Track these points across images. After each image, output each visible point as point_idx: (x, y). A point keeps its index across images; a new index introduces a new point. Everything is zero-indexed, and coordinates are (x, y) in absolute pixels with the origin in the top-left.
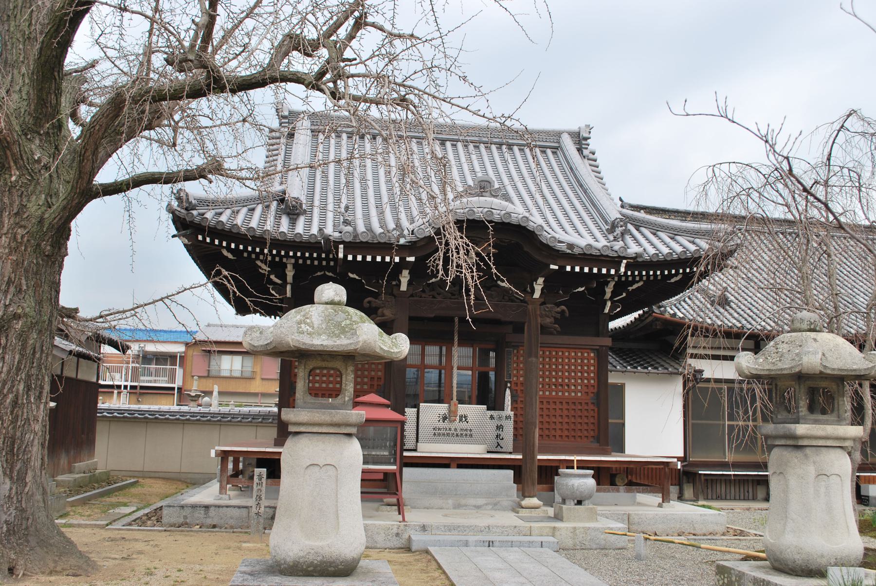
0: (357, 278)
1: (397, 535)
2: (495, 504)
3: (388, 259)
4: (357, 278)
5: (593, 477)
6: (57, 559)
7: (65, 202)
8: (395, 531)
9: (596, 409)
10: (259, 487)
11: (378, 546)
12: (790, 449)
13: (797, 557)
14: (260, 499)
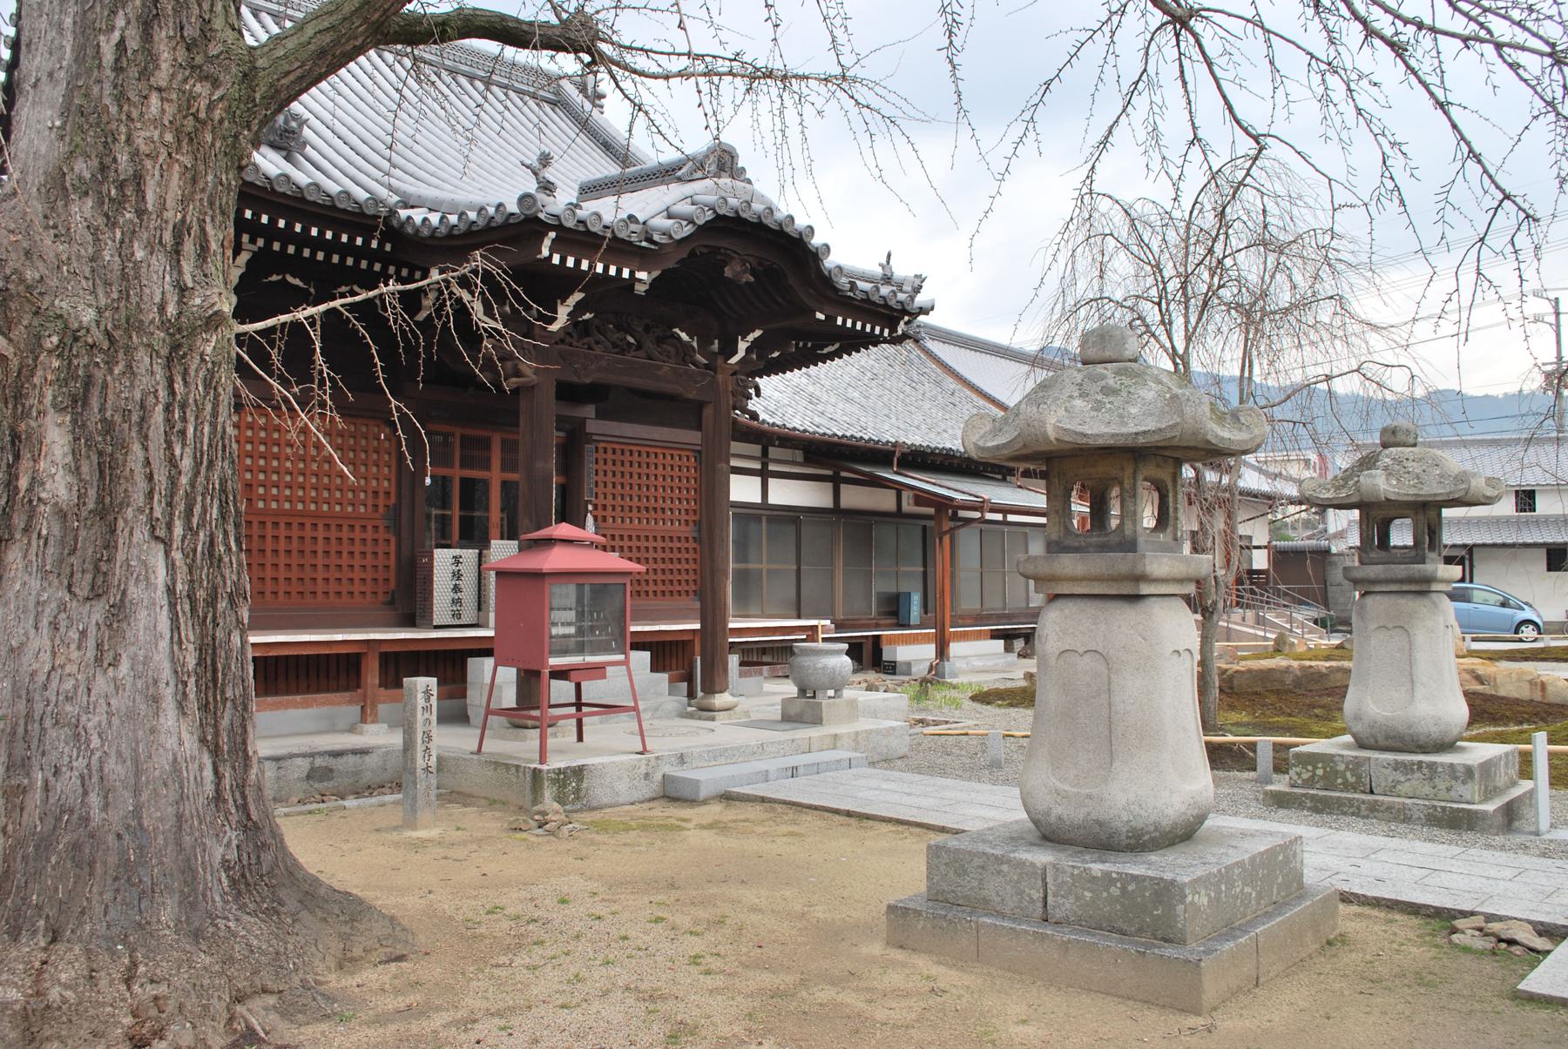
0: (301, 284)
1: (647, 776)
2: (656, 709)
3: (585, 265)
4: (301, 284)
5: (848, 653)
6: (347, 929)
7: (328, 38)
8: (643, 770)
9: (393, 540)
10: (427, 715)
11: (621, 800)
12: (1410, 596)
13: (1433, 729)
14: (430, 737)
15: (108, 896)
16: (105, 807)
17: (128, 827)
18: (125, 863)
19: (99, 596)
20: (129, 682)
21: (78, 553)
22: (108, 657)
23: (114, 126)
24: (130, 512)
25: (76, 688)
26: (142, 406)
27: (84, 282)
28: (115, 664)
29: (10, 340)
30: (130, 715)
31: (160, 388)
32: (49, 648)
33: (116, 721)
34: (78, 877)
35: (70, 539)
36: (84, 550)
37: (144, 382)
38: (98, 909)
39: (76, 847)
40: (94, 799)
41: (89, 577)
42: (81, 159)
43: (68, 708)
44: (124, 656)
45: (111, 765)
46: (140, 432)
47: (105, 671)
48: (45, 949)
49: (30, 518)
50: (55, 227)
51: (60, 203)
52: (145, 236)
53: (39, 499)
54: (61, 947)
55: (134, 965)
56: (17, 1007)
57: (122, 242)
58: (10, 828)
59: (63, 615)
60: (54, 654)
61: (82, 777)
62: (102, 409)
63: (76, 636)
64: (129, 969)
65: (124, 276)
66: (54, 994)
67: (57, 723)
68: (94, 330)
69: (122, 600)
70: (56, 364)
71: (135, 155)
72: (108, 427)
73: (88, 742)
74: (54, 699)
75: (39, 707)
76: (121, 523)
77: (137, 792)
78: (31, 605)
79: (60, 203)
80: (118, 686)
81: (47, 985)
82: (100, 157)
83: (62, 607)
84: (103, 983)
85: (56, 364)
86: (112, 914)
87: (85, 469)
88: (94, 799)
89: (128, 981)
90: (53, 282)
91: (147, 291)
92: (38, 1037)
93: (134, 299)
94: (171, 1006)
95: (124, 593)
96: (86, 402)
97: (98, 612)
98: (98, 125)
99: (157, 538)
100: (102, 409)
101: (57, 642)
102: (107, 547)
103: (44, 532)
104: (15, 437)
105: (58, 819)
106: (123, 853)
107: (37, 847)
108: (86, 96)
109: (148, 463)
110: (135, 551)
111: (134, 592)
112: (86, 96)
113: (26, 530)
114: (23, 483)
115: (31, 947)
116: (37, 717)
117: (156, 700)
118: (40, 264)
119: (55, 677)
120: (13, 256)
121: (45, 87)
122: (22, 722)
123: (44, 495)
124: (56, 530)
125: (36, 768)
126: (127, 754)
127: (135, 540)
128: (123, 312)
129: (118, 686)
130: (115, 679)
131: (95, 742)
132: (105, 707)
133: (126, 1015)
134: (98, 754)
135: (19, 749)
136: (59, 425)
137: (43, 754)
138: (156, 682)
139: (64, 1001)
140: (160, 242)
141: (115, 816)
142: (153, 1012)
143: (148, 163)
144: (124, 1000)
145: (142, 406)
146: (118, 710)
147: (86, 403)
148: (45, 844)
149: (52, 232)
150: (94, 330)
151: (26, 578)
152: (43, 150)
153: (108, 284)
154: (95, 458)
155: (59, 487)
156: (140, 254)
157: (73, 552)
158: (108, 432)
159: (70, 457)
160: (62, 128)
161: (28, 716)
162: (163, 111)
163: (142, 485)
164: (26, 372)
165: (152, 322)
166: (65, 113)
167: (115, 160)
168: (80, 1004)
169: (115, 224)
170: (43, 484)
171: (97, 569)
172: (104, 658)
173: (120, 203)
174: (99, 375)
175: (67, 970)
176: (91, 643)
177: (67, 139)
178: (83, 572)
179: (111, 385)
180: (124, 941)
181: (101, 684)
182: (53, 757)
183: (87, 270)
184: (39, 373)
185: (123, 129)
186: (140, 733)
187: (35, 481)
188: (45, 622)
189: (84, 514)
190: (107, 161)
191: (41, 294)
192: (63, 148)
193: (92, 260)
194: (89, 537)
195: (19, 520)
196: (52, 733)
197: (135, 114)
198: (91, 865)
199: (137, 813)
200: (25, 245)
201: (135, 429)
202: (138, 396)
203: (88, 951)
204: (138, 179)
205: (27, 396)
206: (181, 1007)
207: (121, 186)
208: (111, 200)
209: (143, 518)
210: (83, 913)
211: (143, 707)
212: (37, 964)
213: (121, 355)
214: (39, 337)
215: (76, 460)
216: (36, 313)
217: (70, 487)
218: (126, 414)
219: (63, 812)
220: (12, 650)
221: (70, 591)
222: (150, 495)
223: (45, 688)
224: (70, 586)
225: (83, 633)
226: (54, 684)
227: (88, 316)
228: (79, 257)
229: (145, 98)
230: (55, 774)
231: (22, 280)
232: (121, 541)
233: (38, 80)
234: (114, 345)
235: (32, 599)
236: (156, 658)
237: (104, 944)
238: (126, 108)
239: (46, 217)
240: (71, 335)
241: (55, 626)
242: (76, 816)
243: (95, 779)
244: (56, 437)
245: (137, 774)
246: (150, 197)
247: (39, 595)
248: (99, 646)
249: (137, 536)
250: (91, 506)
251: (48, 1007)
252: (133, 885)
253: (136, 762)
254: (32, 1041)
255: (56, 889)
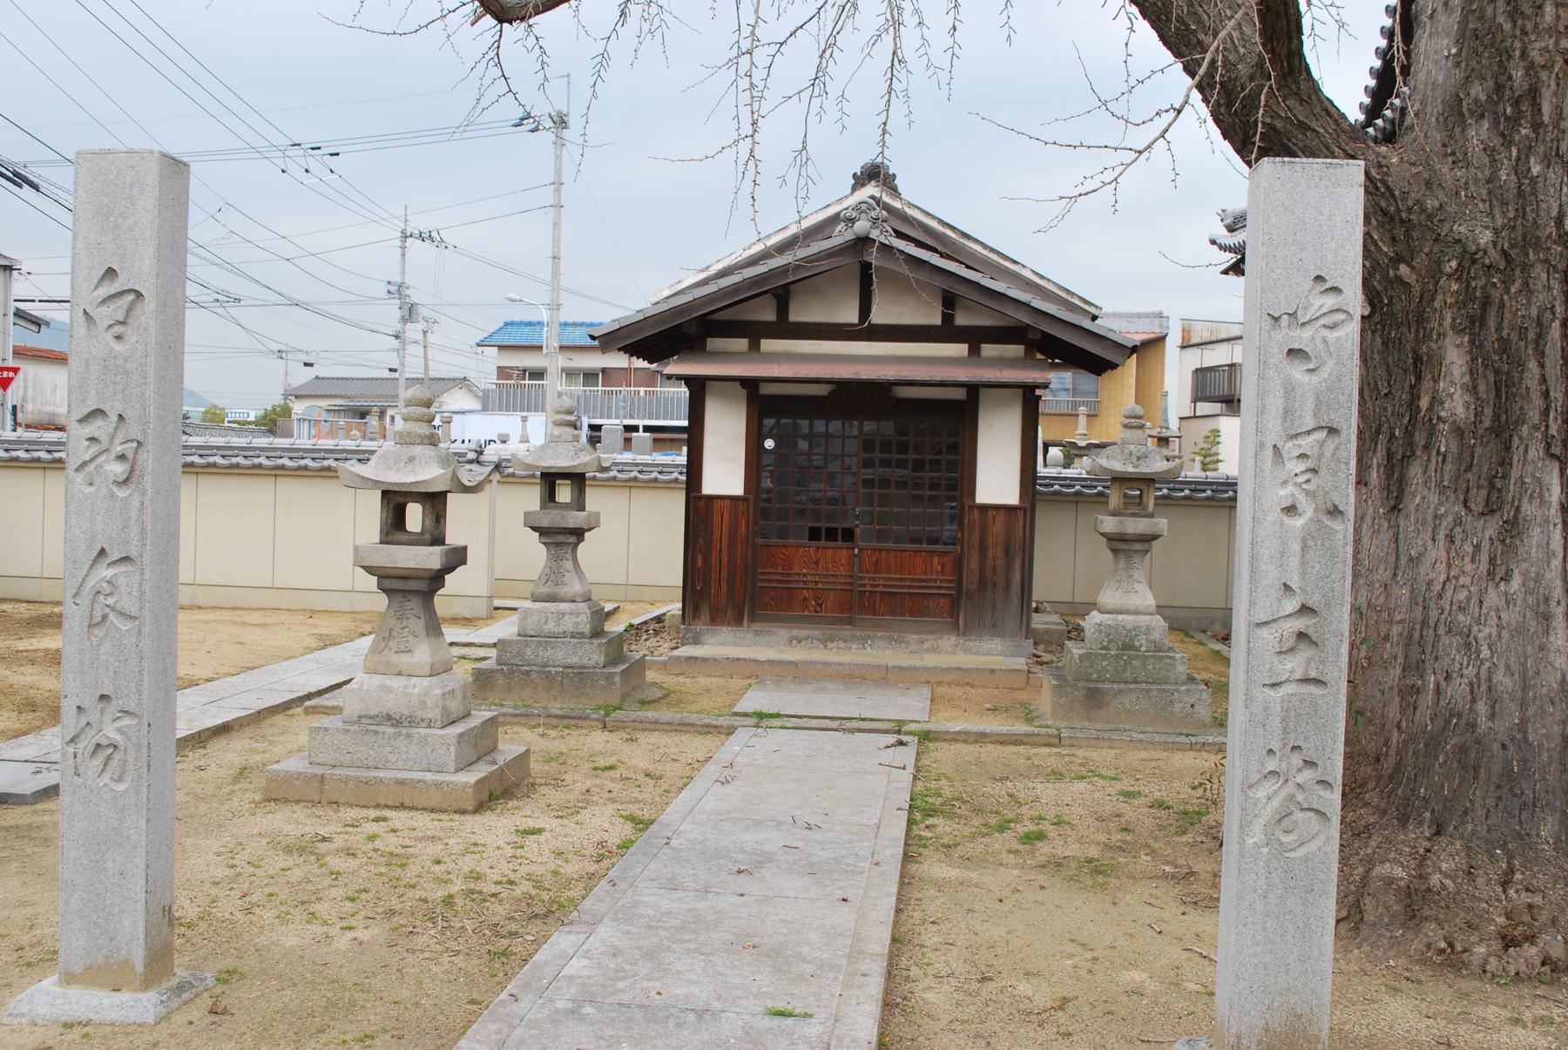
15: (1490, 802)
16: (1492, 716)
17: (1513, 739)
18: (1508, 773)
19: (1493, 511)
20: (1520, 597)
21: (1475, 470)
22: (1500, 572)
23: (1508, 44)
24: (1525, 430)
25: (1468, 599)
26: (1539, 323)
27: (1481, 205)
28: (1506, 578)
29: (1413, 268)
30: (1520, 630)
31: (1557, 303)
32: (1444, 559)
33: (1505, 634)
34: (1463, 779)
35: (1466, 455)
36: (1480, 466)
37: (1541, 298)
38: (1481, 812)
39: (1462, 749)
40: (1482, 707)
41: (1484, 492)
42: (1477, 83)
43: (1461, 618)
44: (1516, 572)
45: (1499, 676)
46: (1536, 349)
47: (1497, 585)
48: (1429, 839)
49: (1430, 436)
50: (1453, 154)
51: (1458, 130)
52: (1541, 149)
53: (1439, 418)
54: (1444, 840)
55: (1511, 871)
56: (1402, 884)
57: (1518, 159)
58: (1404, 724)
59: (1458, 529)
60: (1449, 566)
61: (1471, 684)
62: (1499, 329)
63: (1470, 550)
64: (1506, 874)
65: (1520, 194)
66: (1435, 880)
67: (1450, 631)
68: (1491, 251)
69: (1515, 517)
70: (1455, 287)
71: (1530, 68)
72: (1505, 346)
73: (1478, 652)
74: (1448, 608)
75: (1434, 615)
76: (1516, 441)
77: (1523, 706)
78: (1429, 519)
79: (1458, 130)
80: (1509, 600)
81: (1430, 870)
82: (1496, 76)
83: (1458, 521)
84: (1480, 881)
85: (1455, 287)
86: (1493, 820)
87: (1482, 388)
88: (1482, 707)
89: (1505, 885)
90: (1452, 209)
91: (1544, 206)
92: (1419, 914)
93: (1530, 216)
94: (1544, 917)
95: (1518, 509)
96: (1483, 323)
97: (1491, 528)
98: (1492, 45)
99: (1552, 456)
100: (1499, 329)
101: (1453, 554)
102: (1501, 464)
103: (1443, 449)
104: (1417, 359)
105: (1448, 722)
106: (1507, 763)
107: (1427, 745)
108: (1481, 18)
109: (1543, 380)
110: (1529, 469)
111: (1528, 509)
112: (1481, 18)
113: (1427, 447)
114: (1424, 403)
115: (1417, 835)
116: (1432, 624)
117: (1547, 618)
118: (1440, 193)
119: (1450, 587)
120: (1415, 187)
121: (1442, 18)
122: (1418, 627)
123: (1443, 414)
124: (1454, 448)
125: (1429, 671)
126: (1515, 667)
127: (1530, 457)
128: (1520, 230)
129: (1509, 600)
130: (1506, 593)
131: (1485, 653)
132: (1495, 620)
133: (1499, 915)
134: (1487, 665)
135: (1415, 650)
136: (1457, 346)
137: (1436, 658)
138: (1547, 600)
139: (1444, 887)
140: (1557, 154)
141: (1501, 727)
142: (1526, 918)
143: (1544, 75)
144: (1500, 901)
145: (1539, 323)
146: (1508, 624)
147: (1483, 323)
148: (1435, 743)
149: (1450, 159)
150: (1491, 251)
151: (1426, 492)
152: (1441, 79)
153: (1504, 203)
154: (1491, 377)
155: (1457, 406)
156: (1536, 169)
157: (1469, 468)
158: (1504, 351)
159: (1468, 377)
160: (1458, 54)
161: (1424, 623)
162: (1558, 17)
163: (1538, 402)
164: (1428, 297)
165: (1549, 236)
166: (1460, 40)
167: (1510, 78)
168: (1458, 893)
169: (1510, 143)
170: (1442, 403)
171: (1492, 485)
172: (1497, 573)
173: (1515, 121)
174: (1496, 294)
175: (1446, 864)
176: (1484, 557)
177: (1463, 65)
178: (1479, 487)
179: (1508, 305)
180: (1503, 847)
181: (1492, 598)
182: (1446, 662)
183: (1484, 192)
184: (1439, 297)
185: (1518, 44)
186: (1529, 648)
187: (1436, 401)
188: (1441, 535)
189: (1481, 431)
190: (1502, 79)
191: (1441, 221)
192: (1459, 74)
193: (1489, 181)
194: (1484, 454)
195: (1420, 438)
196: (1445, 640)
197: (1529, 27)
198: (1476, 768)
199: (1523, 725)
200: (1426, 175)
201: (1531, 347)
202: (1534, 313)
203: (1469, 848)
204: (1534, 93)
205: (1428, 320)
206: (1554, 921)
207: (1516, 103)
208: (1507, 119)
209: (1538, 435)
210: (1466, 812)
211: (1533, 623)
212: (1421, 851)
213: (1517, 272)
214: (1439, 263)
215: (1474, 380)
216: (1437, 240)
217: (1467, 406)
218: (1522, 333)
219: (1452, 716)
220: (1411, 559)
221: (1466, 506)
222: (1545, 413)
223: (1440, 597)
224: (1465, 502)
225: (1477, 547)
226: (1448, 594)
227: (1485, 237)
228: (1476, 180)
229: (1540, 7)
230: (1446, 679)
231: (1423, 210)
232: (1516, 458)
233: (1434, 11)
234: (1511, 264)
235: (1430, 513)
236: (1548, 576)
237: (1484, 846)
238: (1520, 22)
239: (1444, 145)
240: (1470, 258)
241: (1450, 539)
242: (1463, 721)
243: (1483, 688)
244: (1455, 358)
245: (1525, 689)
246: (1546, 108)
247: (1436, 509)
248: (1492, 560)
249: (1532, 453)
250: (1487, 424)
251: (1428, 890)
252: (1515, 795)
253: (1524, 676)
254: (1413, 917)
255: (1442, 787)
